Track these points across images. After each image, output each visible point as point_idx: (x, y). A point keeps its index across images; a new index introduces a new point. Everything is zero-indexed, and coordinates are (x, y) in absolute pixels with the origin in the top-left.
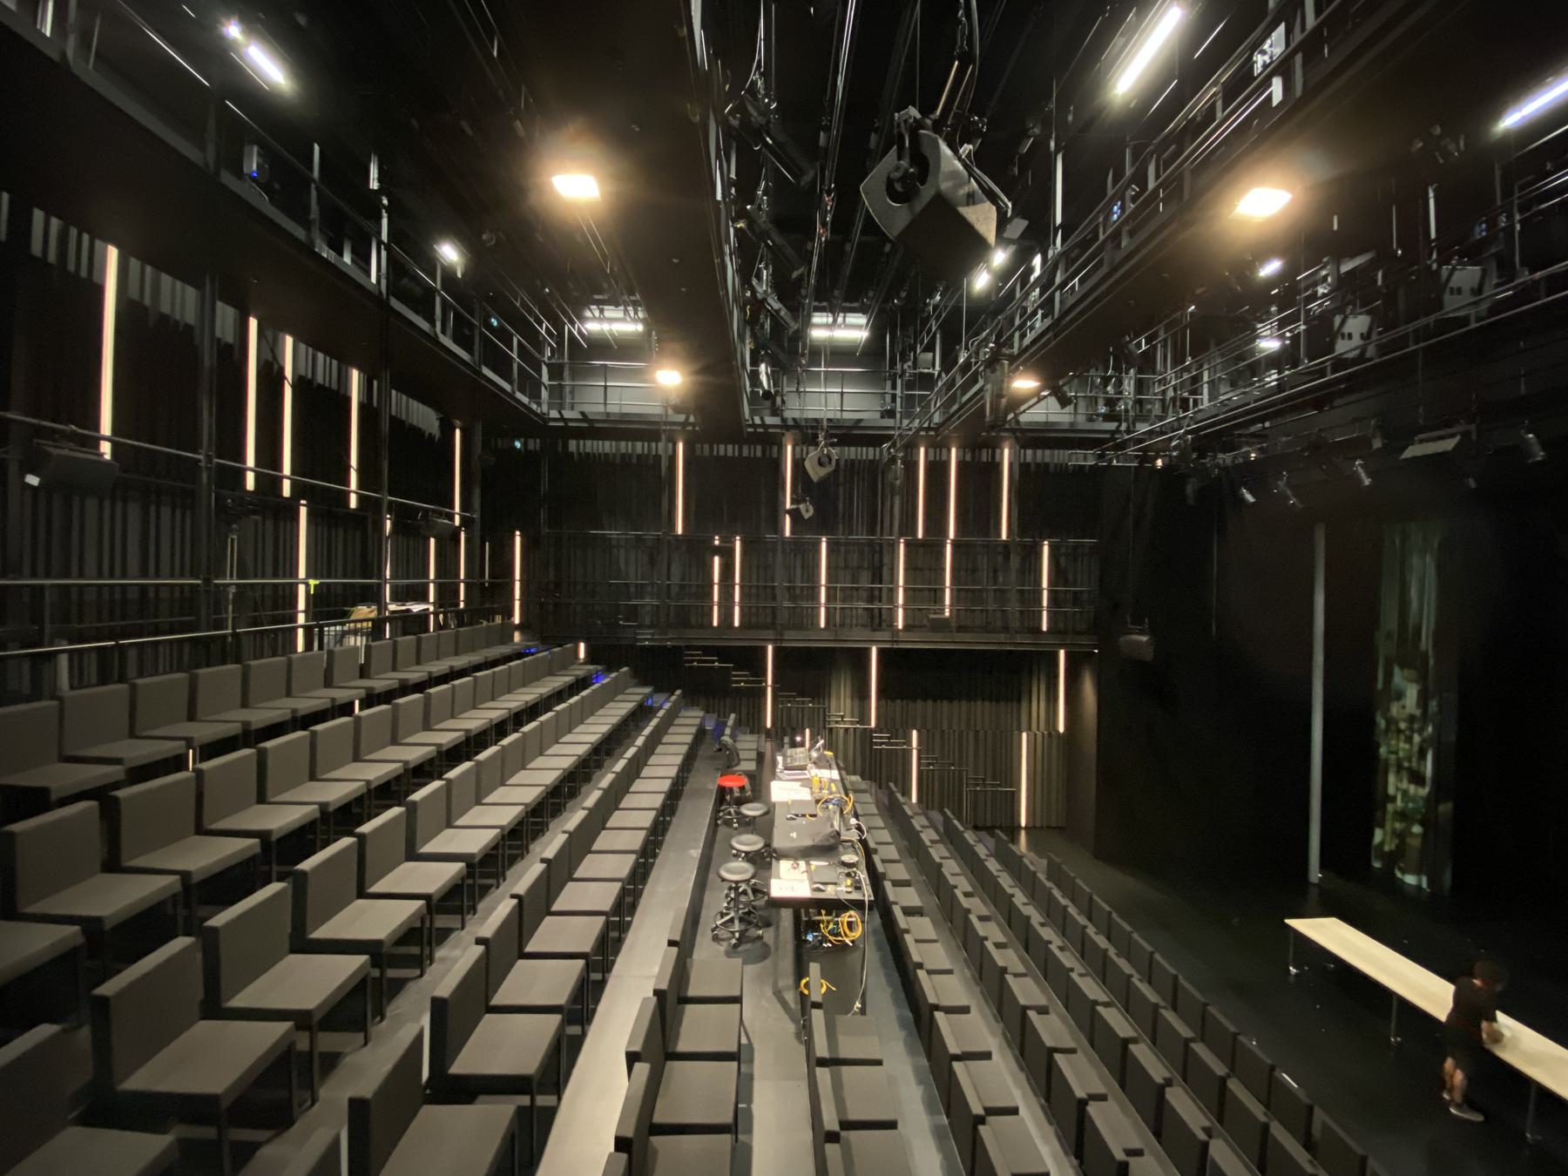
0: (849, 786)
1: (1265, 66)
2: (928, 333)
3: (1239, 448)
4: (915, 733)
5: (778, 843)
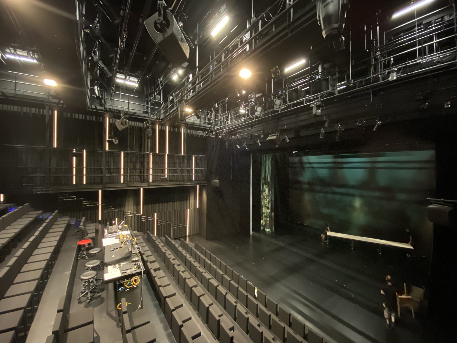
0: (133, 235)
1: (246, 41)
2: (159, 89)
3: (236, 135)
4: (156, 214)
5: (106, 260)
